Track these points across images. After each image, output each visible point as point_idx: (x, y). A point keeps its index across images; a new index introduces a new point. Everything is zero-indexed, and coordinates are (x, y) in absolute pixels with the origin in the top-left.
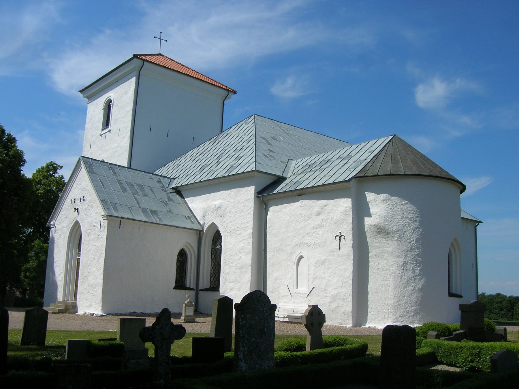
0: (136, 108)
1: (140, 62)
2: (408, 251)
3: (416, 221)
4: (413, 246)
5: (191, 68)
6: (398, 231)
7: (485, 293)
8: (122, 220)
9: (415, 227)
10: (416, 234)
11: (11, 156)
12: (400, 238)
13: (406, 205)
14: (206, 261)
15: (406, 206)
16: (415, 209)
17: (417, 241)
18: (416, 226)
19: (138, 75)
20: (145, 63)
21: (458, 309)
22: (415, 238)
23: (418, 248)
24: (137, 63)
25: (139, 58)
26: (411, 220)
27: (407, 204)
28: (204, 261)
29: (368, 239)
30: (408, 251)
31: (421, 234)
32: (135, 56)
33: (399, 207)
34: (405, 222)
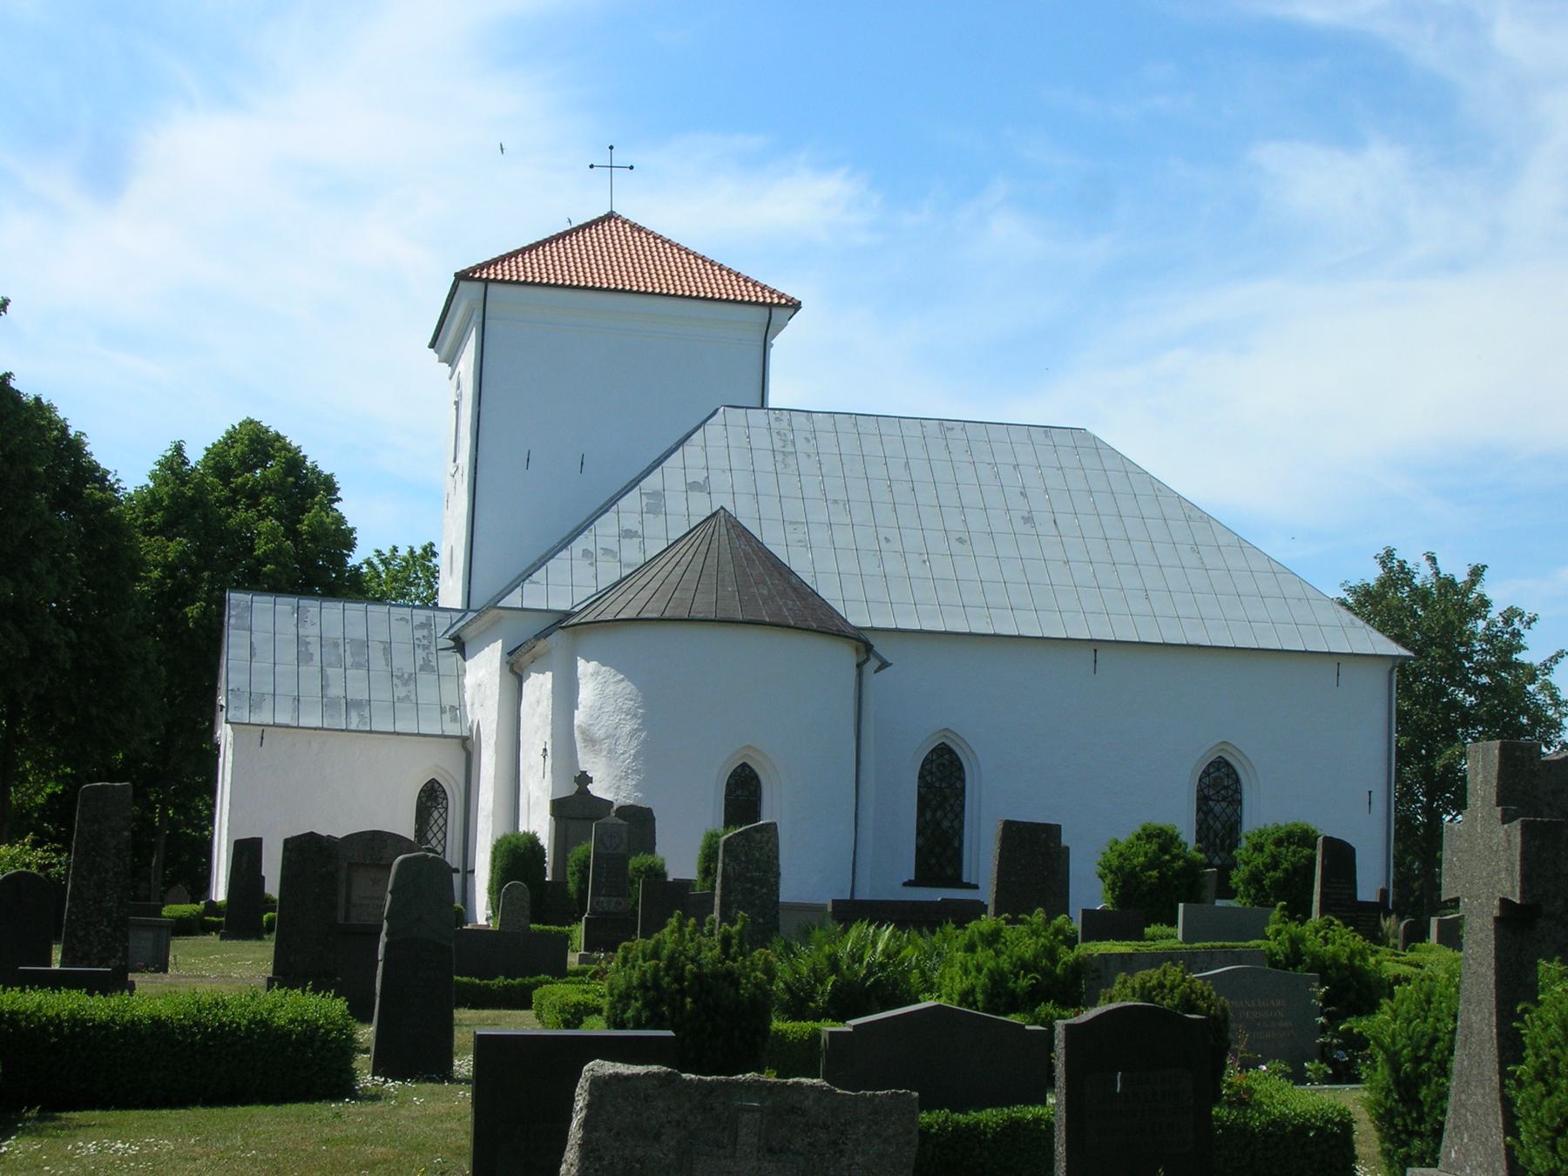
0: (479, 413)
1: (479, 287)
2: (621, 778)
3: (635, 715)
4: (628, 768)
5: (685, 246)
6: (607, 738)
7: (1505, 903)
8: (265, 728)
9: (633, 730)
10: (635, 743)
11: (304, 537)
12: (610, 751)
13: (622, 683)
14: (457, 811)
15: (623, 685)
16: (635, 691)
17: (636, 757)
18: (636, 726)
19: (481, 320)
20: (492, 288)
21: (264, 840)
22: (632, 751)
23: (637, 772)
24: (470, 290)
25: (472, 279)
26: (627, 715)
27: (622, 680)
28: (221, 809)
29: (579, 756)
30: (621, 778)
31: (645, 742)
32: (461, 277)
33: (611, 688)
34: (618, 718)
